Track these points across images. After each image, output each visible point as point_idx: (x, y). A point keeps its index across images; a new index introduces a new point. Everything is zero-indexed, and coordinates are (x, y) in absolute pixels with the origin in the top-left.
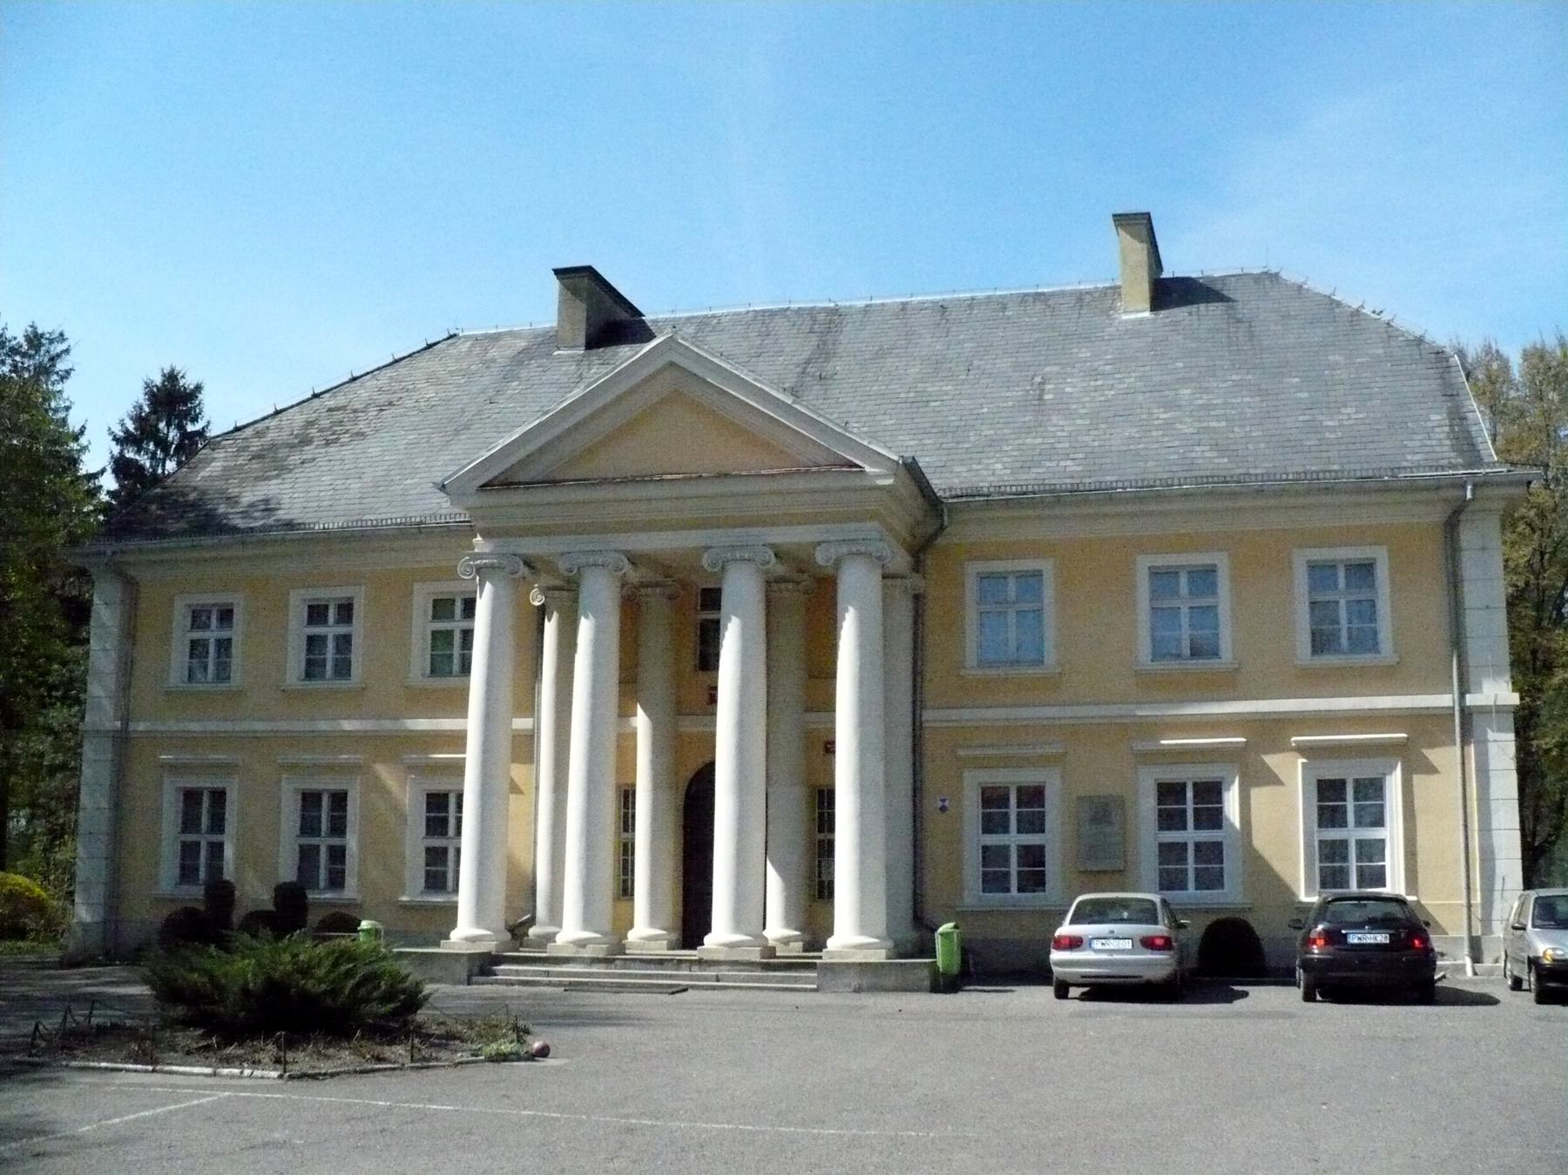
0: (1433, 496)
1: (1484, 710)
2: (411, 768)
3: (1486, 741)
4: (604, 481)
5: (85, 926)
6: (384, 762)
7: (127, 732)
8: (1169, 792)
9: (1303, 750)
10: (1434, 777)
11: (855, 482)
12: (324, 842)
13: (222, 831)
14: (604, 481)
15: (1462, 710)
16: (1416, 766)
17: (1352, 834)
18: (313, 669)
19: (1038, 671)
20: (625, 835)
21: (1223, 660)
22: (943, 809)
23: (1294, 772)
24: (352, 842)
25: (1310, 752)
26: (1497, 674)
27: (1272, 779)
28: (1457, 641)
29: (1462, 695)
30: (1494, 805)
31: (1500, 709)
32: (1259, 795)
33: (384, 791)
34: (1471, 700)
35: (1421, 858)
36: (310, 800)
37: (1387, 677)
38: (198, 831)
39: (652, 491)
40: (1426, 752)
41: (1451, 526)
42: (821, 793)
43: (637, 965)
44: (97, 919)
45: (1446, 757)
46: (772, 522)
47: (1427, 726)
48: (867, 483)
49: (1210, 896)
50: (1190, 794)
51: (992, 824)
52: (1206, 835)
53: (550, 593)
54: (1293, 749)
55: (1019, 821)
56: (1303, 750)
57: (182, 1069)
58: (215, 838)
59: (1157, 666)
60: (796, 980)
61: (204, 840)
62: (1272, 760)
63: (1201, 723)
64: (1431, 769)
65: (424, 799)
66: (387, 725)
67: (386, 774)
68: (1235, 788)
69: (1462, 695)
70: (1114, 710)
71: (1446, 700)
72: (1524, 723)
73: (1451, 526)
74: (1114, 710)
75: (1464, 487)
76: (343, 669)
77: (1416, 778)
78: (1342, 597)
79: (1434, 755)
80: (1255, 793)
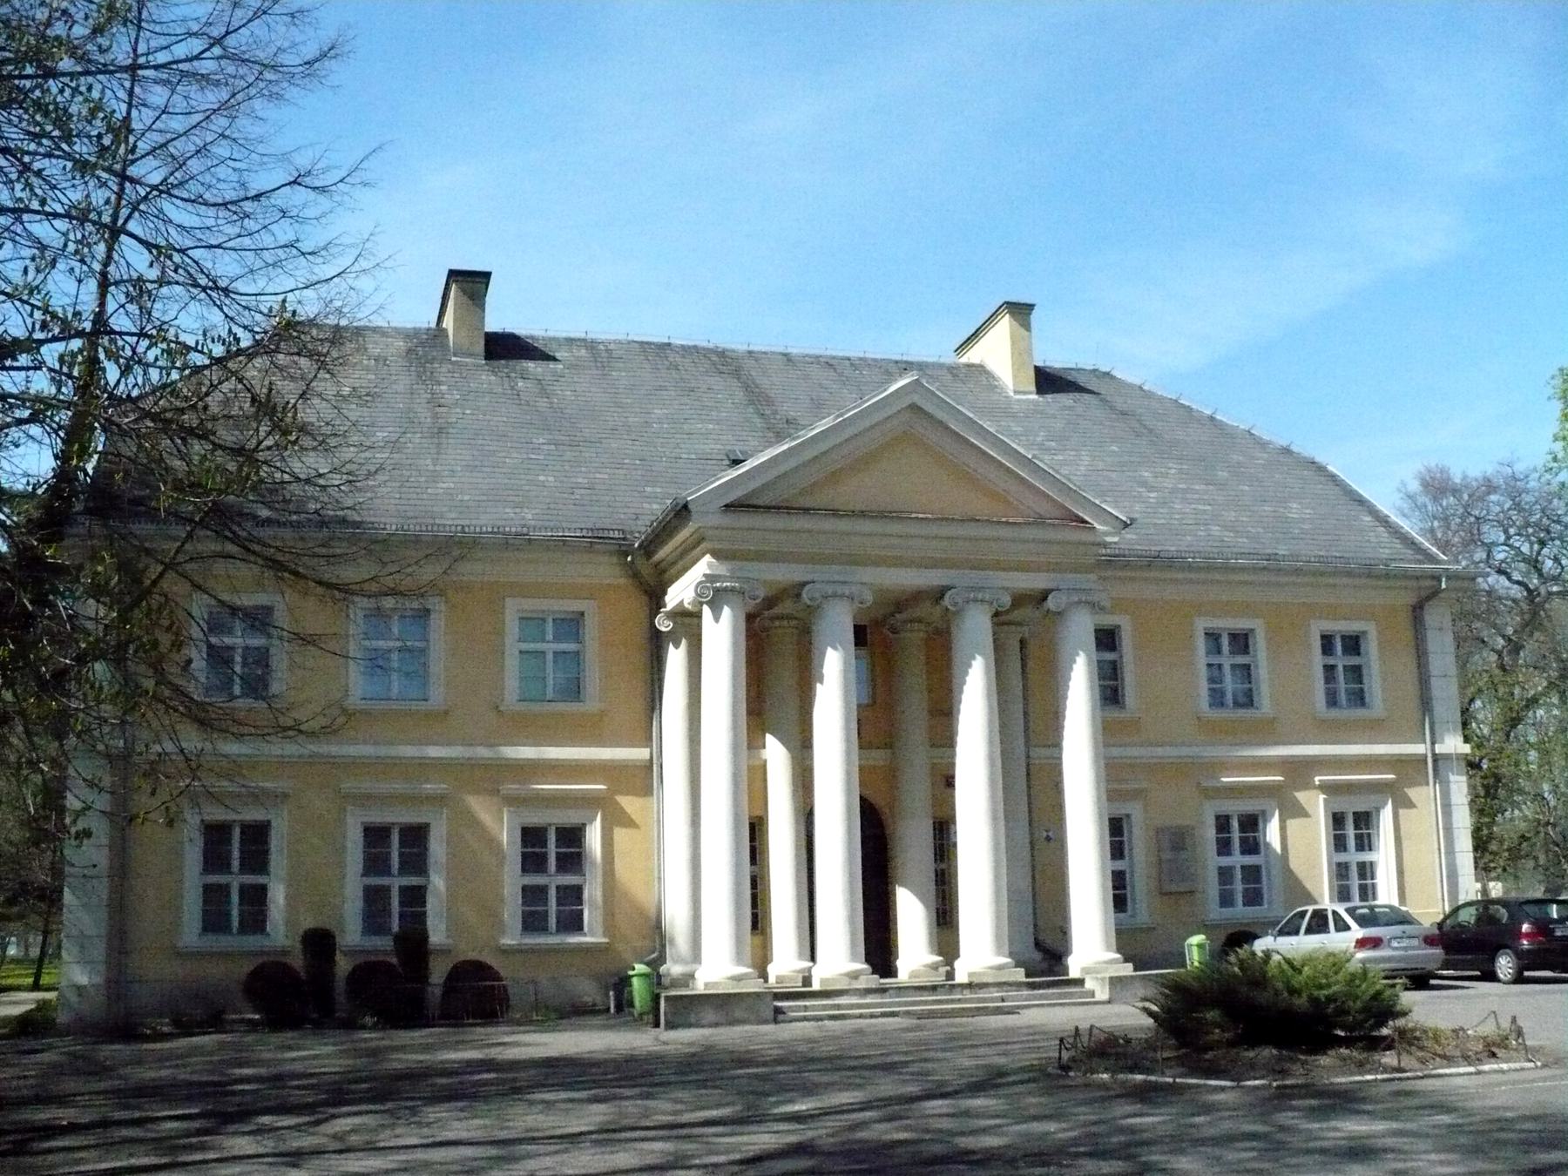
0: (1414, 583)
1: (1447, 757)
2: (514, 801)
3: (1449, 782)
4: (835, 513)
5: (80, 989)
6: (477, 792)
8: (1223, 823)
9: (1326, 788)
11: (1085, 537)
12: (235, 881)
15: (1434, 755)
17: (1237, 859)
19: (423, 706)
20: (943, 866)
22: (1048, 839)
23: (1317, 805)
24: (437, 882)
25: (1330, 789)
27: (1301, 812)
28: (1426, 704)
29: (1433, 743)
30: (1456, 832)
32: (1293, 824)
33: (475, 823)
35: (1406, 874)
36: (375, 835)
37: (1376, 729)
38: (388, 873)
39: (895, 528)
40: (619, 798)
41: (1417, 610)
43: (912, 992)
44: (98, 980)
45: (1424, 795)
47: (1410, 769)
49: (252, 942)
51: (1224, 847)
52: (1250, 860)
53: (679, 620)
54: (1315, 788)
56: (1326, 788)
58: (570, 879)
59: (522, 707)
60: (1065, 996)
62: (1302, 796)
63: (1249, 765)
65: (518, 833)
66: (483, 752)
67: (481, 808)
69: (1433, 743)
70: (1185, 751)
71: (1420, 749)
73: (1417, 610)
74: (1185, 751)
77: (1401, 811)
78: (1340, 661)
79: (1413, 793)
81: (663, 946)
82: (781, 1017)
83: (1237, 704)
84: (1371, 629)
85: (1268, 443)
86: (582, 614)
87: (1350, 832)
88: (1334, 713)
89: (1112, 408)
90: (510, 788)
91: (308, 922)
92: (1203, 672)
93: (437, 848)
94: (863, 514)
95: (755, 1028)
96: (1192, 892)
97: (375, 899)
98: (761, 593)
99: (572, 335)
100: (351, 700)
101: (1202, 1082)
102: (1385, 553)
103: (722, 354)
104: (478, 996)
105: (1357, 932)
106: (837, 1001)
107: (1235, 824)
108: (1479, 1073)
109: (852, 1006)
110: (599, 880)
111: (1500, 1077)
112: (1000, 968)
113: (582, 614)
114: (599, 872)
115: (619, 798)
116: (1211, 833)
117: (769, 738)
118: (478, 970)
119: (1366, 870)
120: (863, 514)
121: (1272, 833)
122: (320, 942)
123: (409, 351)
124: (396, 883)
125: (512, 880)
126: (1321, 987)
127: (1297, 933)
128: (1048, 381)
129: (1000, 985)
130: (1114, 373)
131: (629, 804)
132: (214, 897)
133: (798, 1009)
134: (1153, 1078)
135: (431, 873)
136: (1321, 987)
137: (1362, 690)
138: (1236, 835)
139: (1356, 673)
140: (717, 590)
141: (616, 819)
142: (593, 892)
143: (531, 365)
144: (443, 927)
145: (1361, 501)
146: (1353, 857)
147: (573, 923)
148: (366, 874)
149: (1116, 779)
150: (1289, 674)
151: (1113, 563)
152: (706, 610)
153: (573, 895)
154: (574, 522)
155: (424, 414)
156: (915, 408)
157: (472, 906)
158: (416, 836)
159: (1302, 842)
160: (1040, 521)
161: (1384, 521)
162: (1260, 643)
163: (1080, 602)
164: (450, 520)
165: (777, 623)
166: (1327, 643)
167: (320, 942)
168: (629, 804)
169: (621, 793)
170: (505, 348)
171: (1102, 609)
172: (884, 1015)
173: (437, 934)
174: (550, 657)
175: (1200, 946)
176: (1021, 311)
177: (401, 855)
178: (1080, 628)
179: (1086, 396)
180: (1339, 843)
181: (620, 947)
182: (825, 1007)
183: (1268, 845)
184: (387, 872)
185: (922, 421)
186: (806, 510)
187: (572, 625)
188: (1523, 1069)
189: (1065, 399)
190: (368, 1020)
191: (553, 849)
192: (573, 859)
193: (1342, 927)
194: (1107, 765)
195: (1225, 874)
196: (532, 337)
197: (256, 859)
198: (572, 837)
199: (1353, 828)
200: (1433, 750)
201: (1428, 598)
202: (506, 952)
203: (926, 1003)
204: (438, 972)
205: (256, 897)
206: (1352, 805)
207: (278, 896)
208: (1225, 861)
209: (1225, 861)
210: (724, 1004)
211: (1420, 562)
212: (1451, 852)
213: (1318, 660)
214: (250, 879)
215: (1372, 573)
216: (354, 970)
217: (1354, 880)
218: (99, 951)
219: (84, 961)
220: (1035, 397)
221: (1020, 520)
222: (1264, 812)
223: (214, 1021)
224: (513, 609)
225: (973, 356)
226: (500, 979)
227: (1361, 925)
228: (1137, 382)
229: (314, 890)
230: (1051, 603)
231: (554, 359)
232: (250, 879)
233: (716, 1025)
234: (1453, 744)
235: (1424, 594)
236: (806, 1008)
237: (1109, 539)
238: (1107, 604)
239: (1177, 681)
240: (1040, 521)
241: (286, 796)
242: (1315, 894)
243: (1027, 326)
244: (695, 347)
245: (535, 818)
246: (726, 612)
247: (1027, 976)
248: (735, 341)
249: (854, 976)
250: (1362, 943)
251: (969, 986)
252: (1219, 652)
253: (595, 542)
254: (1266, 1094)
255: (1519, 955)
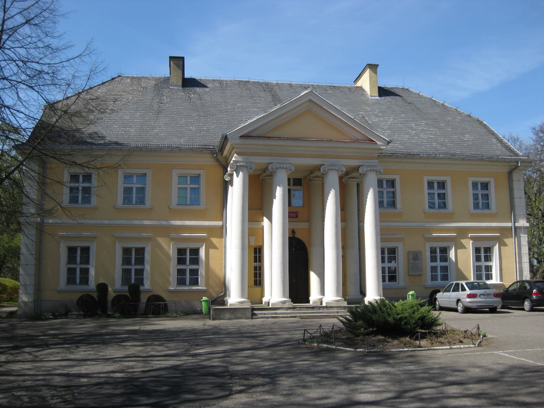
0: (508, 164)
1: (520, 228)
2: (173, 239)
4: (280, 138)
5: (25, 303)
7: (43, 222)
8: (433, 251)
9: (472, 238)
10: (506, 247)
13: (88, 262)
14: (280, 138)
16: (502, 244)
17: (439, 264)
18: (127, 199)
21: (92, 204)
23: (470, 245)
24: (147, 267)
26: (523, 218)
27: (463, 247)
28: (512, 208)
29: (515, 223)
31: (525, 228)
34: (517, 225)
40: (211, 239)
41: (510, 173)
42: (255, 249)
45: (510, 241)
46: (343, 157)
47: (505, 232)
48: (378, 147)
49: (84, 287)
50: (438, 251)
51: (433, 259)
55: (440, 259)
57: (441, 347)
58: (194, 267)
61: (78, 267)
62: (463, 241)
64: (505, 245)
66: (164, 223)
67: (162, 241)
68: (453, 249)
69: (515, 223)
70: (419, 224)
71: (509, 225)
72: (530, 231)
73: (510, 173)
75: (518, 162)
76: (141, 201)
77: (502, 247)
78: (480, 192)
79: (506, 241)
80: (459, 251)
81: (226, 290)
82: (254, 317)
83: (440, 207)
84: (397, 178)
85: (462, 113)
86: (200, 175)
87: (483, 255)
88: (477, 211)
89: (406, 102)
90: (174, 235)
91: (102, 281)
92: (426, 197)
93: (147, 256)
94: (291, 139)
95: (236, 321)
96: (421, 275)
97: (126, 273)
98: (344, 170)
99: (215, 79)
100: (64, 204)
101: (344, 348)
102: (498, 153)
103: (267, 84)
104: (158, 307)
105: (468, 291)
106: (278, 311)
107: (438, 251)
108: (451, 348)
109: (282, 314)
110: (204, 268)
111: (459, 350)
112: (338, 301)
113: (200, 175)
114: (204, 265)
115: (211, 239)
116: (428, 254)
117: (265, 218)
118: (158, 298)
119: (489, 269)
120: (291, 139)
121: (452, 254)
122: (102, 288)
123: (156, 85)
124: (133, 268)
125: (173, 267)
126: (398, 314)
127: (449, 291)
128: (383, 92)
129: (338, 307)
130: (410, 89)
131: (215, 240)
132: (71, 272)
133: (262, 314)
134: (329, 346)
135: (145, 264)
136: (398, 314)
137: (488, 203)
138: (438, 255)
139: (486, 197)
140: (237, 166)
141: (210, 246)
142: (202, 271)
143: (198, 89)
144: (149, 283)
145: (493, 134)
146: (483, 264)
147: (195, 282)
148: (123, 265)
149: (382, 233)
150: (459, 197)
151: (382, 156)
152: (235, 173)
153: (195, 272)
154: (198, 142)
155: (156, 106)
156: (310, 100)
157: (160, 276)
158: (140, 251)
159: (463, 258)
160: (357, 141)
161: (501, 141)
162: (449, 186)
163: (371, 170)
164: (154, 142)
165: (268, 178)
166: (475, 185)
167: (102, 288)
168: (215, 240)
169: (506, 238)
170: (190, 83)
171: (380, 172)
172: (291, 317)
173: (147, 285)
174: (189, 190)
175: (412, 295)
176: (373, 67)
177: (135, 258)
178: (371, 179)
179: (397, 97)
180: (478, 259)
181: (211, 290)
182: (272, 314)
183: (450, 259)
184: (75, 263)
185: (312, 105)
186: (269, 138)
187: (196, 179)
188: (469, 347)
189: (389, 98)
190: (117, 315)
191: (188, 257)
192: (195, 260)
193: (463, 289)
194: (381, 229)
195: (434, 269)
196: (201, 80)
197: (86, 260)
198: (195, 252)
199: (483, 254)
200: (514, 225)
201: (514, 169)
202: (171, 292)
203: (309, 313)
204: (144, 299)
205: (85, 272)
206: (483, 245)
207: (92, 272)
208: (434, 264)
209: (434, 264)
210: (235, 312)
211: (511, 156)
212: (520, 263)
213: (471, 192)
214: (83, 266)
215: (492, 160)
216: (115, 297)
217: (483, 272)
218: (31, 290)
219: (27, 293)
220: (378, 98)
221: (349, 141)
222: (449, 247)
223: (66, 315)
224: (175, 174)
225: (359, 84)
226: (165, 301)
227: (470, 289)
228: (417, 92)
229: (106, 271)
230: (360, 170)
231: (206, 87)
232: (83, 266)
233: (230, 319)
234: (523, 223)
235: (513, 167)
236: (265, 314)
237: (382, 147)
238: (382, 171)
239: (414, 199)
240: (357, 141)
241: (151, 238)
242: (468, 277)
243: (376, 73)
244: (258, 82)
245: (182, 246)
246: (241, 174)
247: (348, 304)
248: (272, 78)
249: (284, 302)
250: (469, 296)
251: (326, 307)
252: (477, 189)
253: (204, 150)
254: (361, 354)
255: (532, 301)
